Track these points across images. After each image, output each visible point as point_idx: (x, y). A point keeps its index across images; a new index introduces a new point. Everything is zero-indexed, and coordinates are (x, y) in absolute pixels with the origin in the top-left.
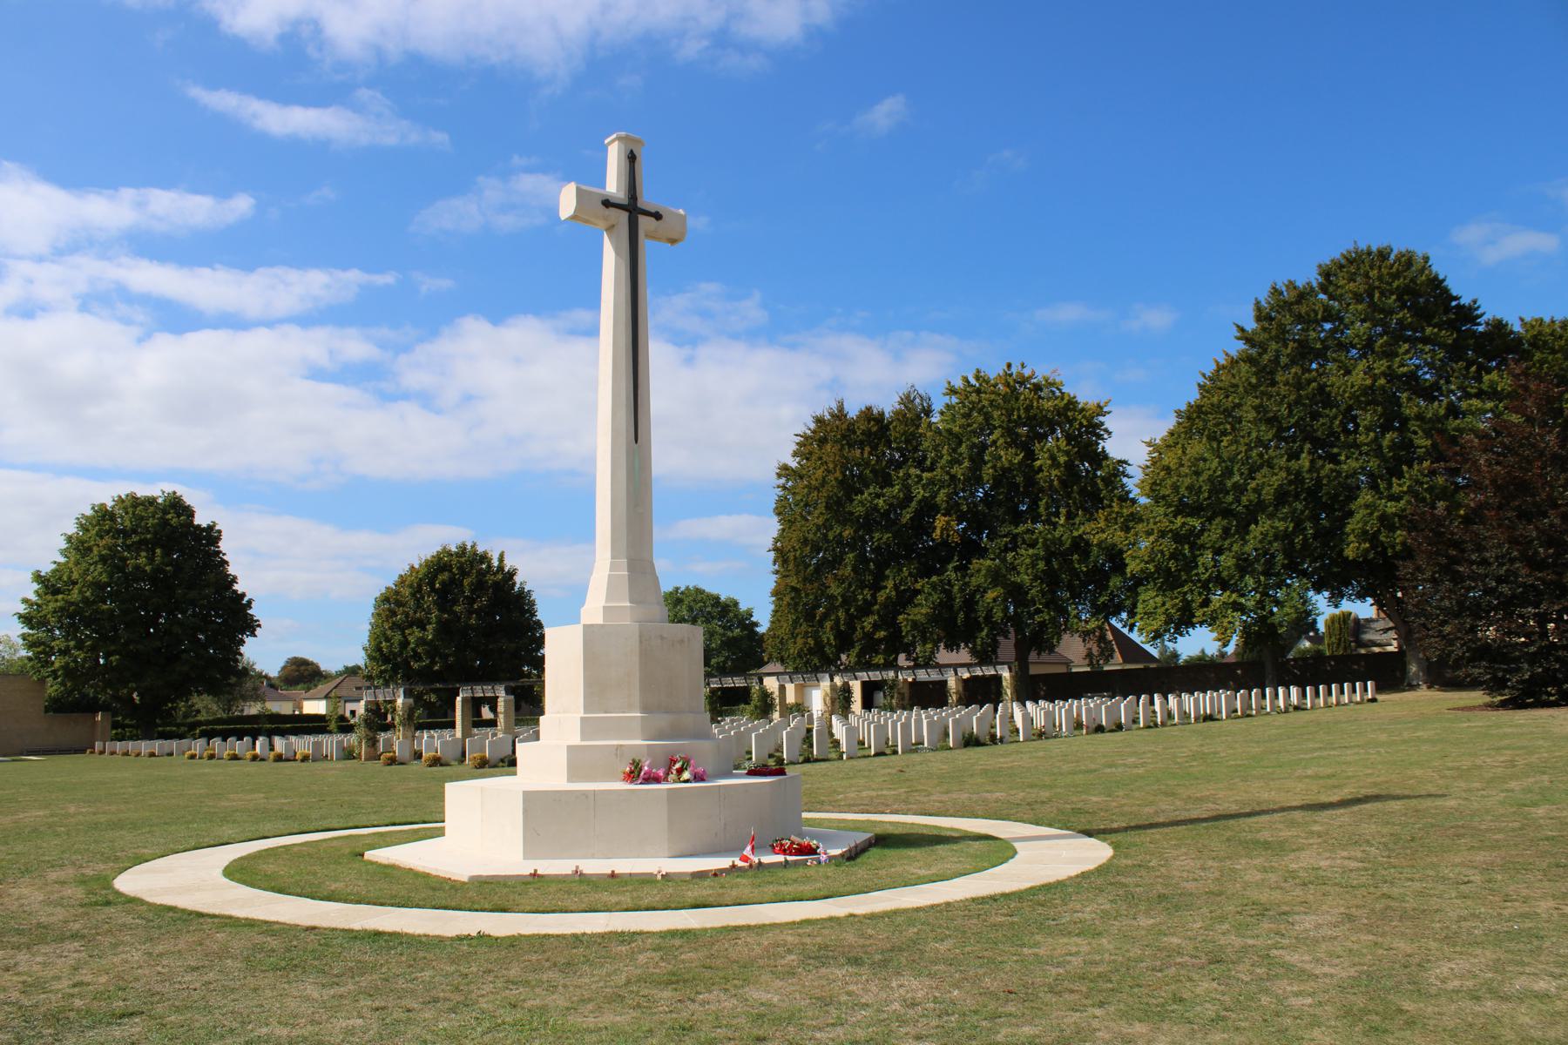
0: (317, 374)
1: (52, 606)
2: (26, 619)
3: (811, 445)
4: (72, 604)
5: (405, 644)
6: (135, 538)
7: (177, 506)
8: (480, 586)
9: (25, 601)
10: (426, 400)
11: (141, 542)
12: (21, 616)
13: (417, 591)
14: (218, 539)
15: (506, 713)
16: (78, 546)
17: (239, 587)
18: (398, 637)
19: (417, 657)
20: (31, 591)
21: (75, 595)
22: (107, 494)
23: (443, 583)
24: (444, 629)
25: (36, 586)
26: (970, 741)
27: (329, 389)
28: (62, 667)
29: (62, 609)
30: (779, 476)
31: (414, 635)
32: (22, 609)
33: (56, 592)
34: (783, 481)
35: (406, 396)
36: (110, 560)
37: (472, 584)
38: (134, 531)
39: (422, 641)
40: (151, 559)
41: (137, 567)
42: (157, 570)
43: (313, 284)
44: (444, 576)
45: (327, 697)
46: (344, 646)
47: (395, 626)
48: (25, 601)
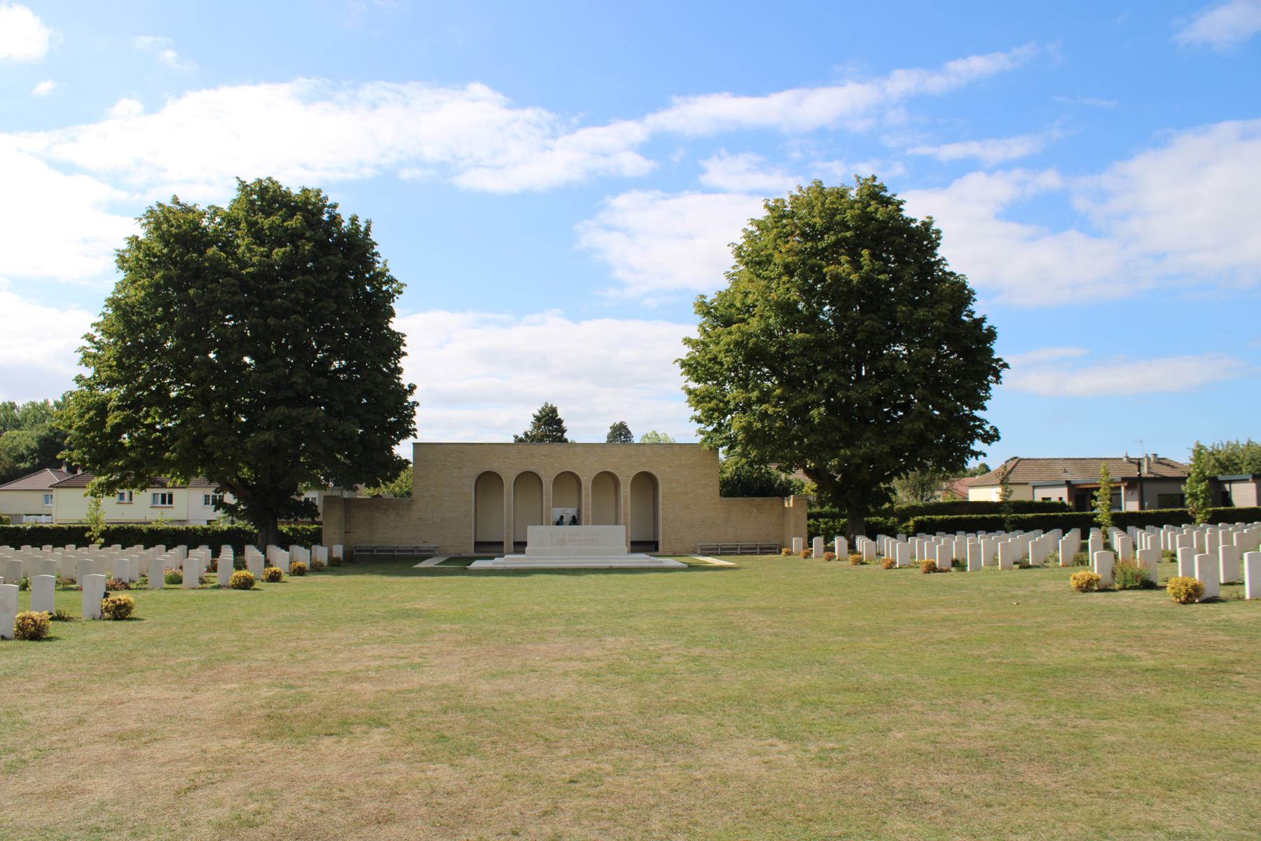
1: (725, 339)
2: (690, 367)
3: (138, 261)
4: (750, 335)
6: (830, 239)
9: (688, 341)
11: (837, 244)
12: (684, 364)
14: (934, 245)
16: (754, 260)
20: (533, 419)
22: (786, 185)
25: (700, 319)
28: (744, 429)
29: (737, 344)
32: (684, 352)
33: (728, 322)
36: (806, 268)
38: (827, 230)
40: (857, 266)
41: (836, 278)
42: (867, 281)
43: (1018, 147)
48: (688, 341)
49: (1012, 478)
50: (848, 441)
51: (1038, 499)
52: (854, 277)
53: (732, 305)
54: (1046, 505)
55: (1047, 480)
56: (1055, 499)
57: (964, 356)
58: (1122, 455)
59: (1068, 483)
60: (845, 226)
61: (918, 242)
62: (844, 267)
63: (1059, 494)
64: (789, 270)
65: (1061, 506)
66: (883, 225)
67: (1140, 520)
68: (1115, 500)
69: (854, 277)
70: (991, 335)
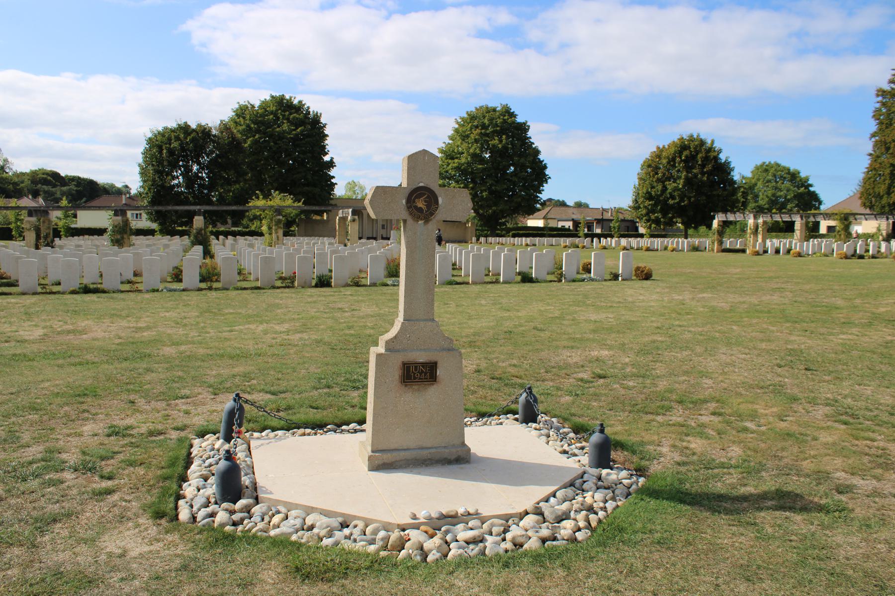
0: (481, 34)
5: (665, 189)
6: (490, 129)
7: (508, 112)
8: (706, 159)
10: (540, 47)
11: (494, 132)
13: (672, 161)
15: (801, 230)
17: (541, 157)
18: (660, 187)
19: (673, 198)
21: (463, 160)
23: (686, 157)
24: (688, 182)
26: (648, 249)
27: (487, 43)
30: (878, 96)
31: (671, 185)
34: (880, 99)
35: (527, 45)
37: (701, 158)
39: (676, 189)
40: (501, 141)
42: (505, 148)
44: (686, 153)
45: (544, 218)
46: (618, 194)
47: (658, 180)
49: (549, 216)
50: (496, 204)
51: (560, 226)
52: (500, 146)
53: (453, 151)
54: (563, 229)
55: (565, 218)
56: (567, 227)
57: (537, 173)
58: (599, 207)
59: (573, 220)
60: (497, 125)
61: (523, 128)
62: (496, 141)
63: (569, 225)
64: (476, 141)
65: (569, 230)
66: (511, 124)
67: (599, 236)
68: (590, 227)
69: (500, 146)
70: (545, 167)
